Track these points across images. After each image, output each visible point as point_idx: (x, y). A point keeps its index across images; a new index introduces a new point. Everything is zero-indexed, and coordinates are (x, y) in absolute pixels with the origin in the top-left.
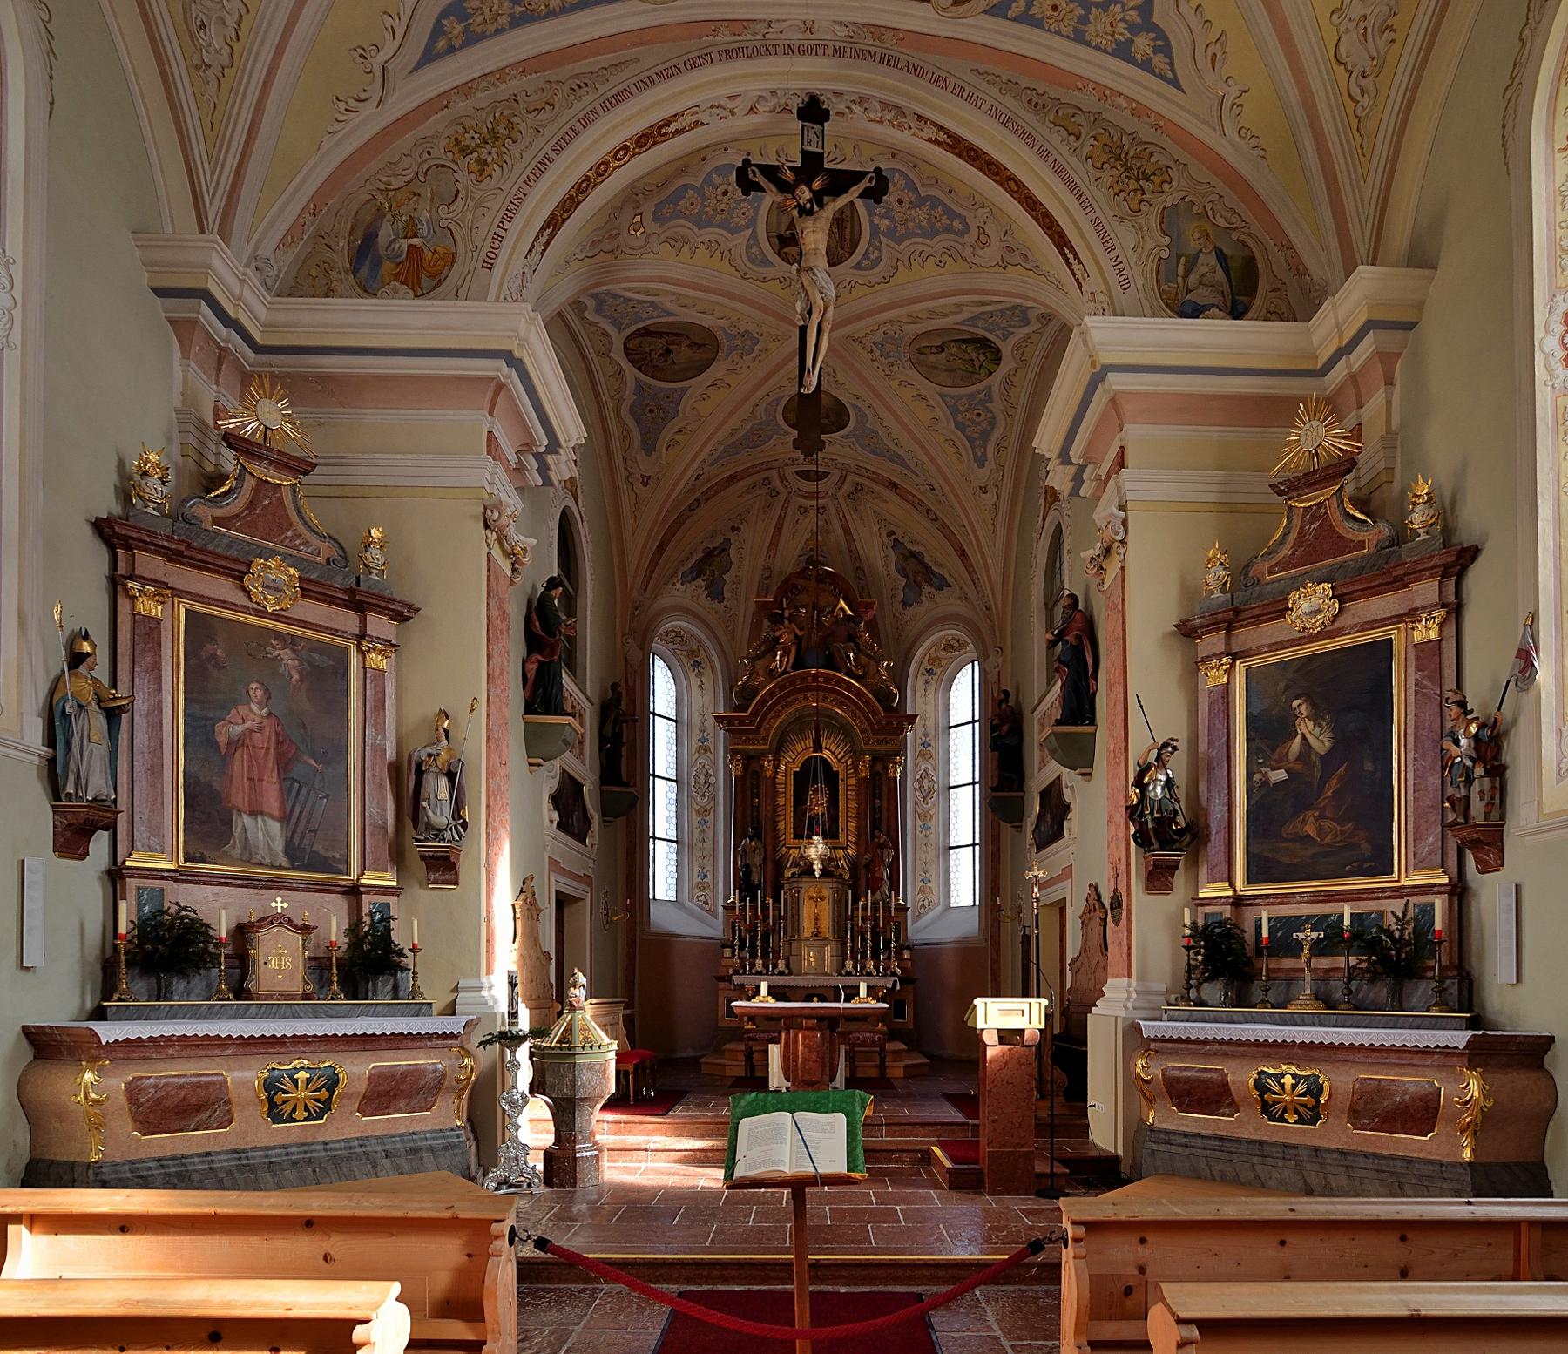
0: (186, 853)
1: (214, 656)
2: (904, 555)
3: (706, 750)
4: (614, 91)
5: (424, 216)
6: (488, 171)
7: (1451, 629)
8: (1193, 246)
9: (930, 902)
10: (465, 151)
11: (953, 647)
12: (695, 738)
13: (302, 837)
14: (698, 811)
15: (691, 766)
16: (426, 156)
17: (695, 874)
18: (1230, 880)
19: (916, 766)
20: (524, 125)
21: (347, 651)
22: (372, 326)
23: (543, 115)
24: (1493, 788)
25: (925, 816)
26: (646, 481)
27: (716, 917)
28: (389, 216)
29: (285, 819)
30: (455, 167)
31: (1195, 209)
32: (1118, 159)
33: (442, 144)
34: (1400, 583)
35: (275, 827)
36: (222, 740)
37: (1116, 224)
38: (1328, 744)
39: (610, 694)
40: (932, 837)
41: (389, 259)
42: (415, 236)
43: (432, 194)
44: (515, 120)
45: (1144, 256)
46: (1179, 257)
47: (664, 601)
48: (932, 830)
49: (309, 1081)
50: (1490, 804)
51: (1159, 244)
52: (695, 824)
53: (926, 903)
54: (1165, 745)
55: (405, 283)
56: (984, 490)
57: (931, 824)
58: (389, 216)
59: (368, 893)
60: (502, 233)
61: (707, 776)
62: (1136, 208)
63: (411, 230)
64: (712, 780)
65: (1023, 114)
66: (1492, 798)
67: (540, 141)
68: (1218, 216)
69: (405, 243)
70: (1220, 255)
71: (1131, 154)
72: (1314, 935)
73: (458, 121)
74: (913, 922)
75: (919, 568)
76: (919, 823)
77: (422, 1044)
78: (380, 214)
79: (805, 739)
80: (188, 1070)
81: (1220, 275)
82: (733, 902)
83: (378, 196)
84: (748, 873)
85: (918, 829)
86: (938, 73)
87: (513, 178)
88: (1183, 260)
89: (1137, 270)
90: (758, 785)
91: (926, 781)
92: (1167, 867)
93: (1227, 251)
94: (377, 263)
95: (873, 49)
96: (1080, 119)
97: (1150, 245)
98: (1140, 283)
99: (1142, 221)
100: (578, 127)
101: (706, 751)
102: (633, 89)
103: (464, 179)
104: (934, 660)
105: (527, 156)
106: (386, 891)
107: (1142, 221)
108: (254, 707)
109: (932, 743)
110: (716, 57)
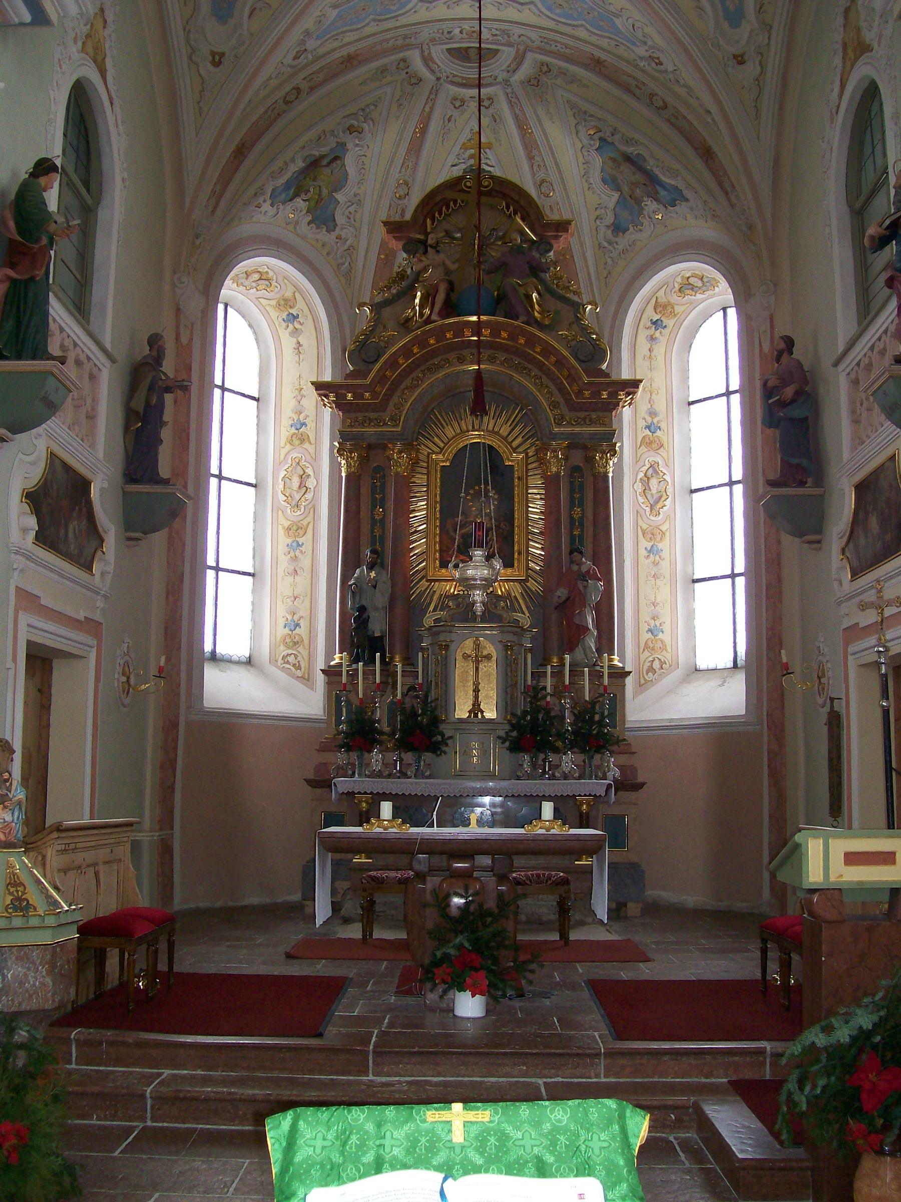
2: (614, 160)
3: (303, 439)
12: (286, 422)
14: (289, 529)
15: (278, 464)
17: (281, 622)
19: (637, 460)
25: (653, 534)
26: (217, 60)
27: (312, 687)
40: (665, 565)
47: (246, 228)
48: (665, 554)
52: (282, 548)
53: (656, 665)
56: (740, 60)
57: (664, 545)
61: (303, 477)
64: (311, 483)
74: (635, 695)
75: (639, 177)
76: (644, 544)
82: (340, 665)
85: (643, 553)
91: (654, 482)
104: (665, 307)
109: (663, 425)
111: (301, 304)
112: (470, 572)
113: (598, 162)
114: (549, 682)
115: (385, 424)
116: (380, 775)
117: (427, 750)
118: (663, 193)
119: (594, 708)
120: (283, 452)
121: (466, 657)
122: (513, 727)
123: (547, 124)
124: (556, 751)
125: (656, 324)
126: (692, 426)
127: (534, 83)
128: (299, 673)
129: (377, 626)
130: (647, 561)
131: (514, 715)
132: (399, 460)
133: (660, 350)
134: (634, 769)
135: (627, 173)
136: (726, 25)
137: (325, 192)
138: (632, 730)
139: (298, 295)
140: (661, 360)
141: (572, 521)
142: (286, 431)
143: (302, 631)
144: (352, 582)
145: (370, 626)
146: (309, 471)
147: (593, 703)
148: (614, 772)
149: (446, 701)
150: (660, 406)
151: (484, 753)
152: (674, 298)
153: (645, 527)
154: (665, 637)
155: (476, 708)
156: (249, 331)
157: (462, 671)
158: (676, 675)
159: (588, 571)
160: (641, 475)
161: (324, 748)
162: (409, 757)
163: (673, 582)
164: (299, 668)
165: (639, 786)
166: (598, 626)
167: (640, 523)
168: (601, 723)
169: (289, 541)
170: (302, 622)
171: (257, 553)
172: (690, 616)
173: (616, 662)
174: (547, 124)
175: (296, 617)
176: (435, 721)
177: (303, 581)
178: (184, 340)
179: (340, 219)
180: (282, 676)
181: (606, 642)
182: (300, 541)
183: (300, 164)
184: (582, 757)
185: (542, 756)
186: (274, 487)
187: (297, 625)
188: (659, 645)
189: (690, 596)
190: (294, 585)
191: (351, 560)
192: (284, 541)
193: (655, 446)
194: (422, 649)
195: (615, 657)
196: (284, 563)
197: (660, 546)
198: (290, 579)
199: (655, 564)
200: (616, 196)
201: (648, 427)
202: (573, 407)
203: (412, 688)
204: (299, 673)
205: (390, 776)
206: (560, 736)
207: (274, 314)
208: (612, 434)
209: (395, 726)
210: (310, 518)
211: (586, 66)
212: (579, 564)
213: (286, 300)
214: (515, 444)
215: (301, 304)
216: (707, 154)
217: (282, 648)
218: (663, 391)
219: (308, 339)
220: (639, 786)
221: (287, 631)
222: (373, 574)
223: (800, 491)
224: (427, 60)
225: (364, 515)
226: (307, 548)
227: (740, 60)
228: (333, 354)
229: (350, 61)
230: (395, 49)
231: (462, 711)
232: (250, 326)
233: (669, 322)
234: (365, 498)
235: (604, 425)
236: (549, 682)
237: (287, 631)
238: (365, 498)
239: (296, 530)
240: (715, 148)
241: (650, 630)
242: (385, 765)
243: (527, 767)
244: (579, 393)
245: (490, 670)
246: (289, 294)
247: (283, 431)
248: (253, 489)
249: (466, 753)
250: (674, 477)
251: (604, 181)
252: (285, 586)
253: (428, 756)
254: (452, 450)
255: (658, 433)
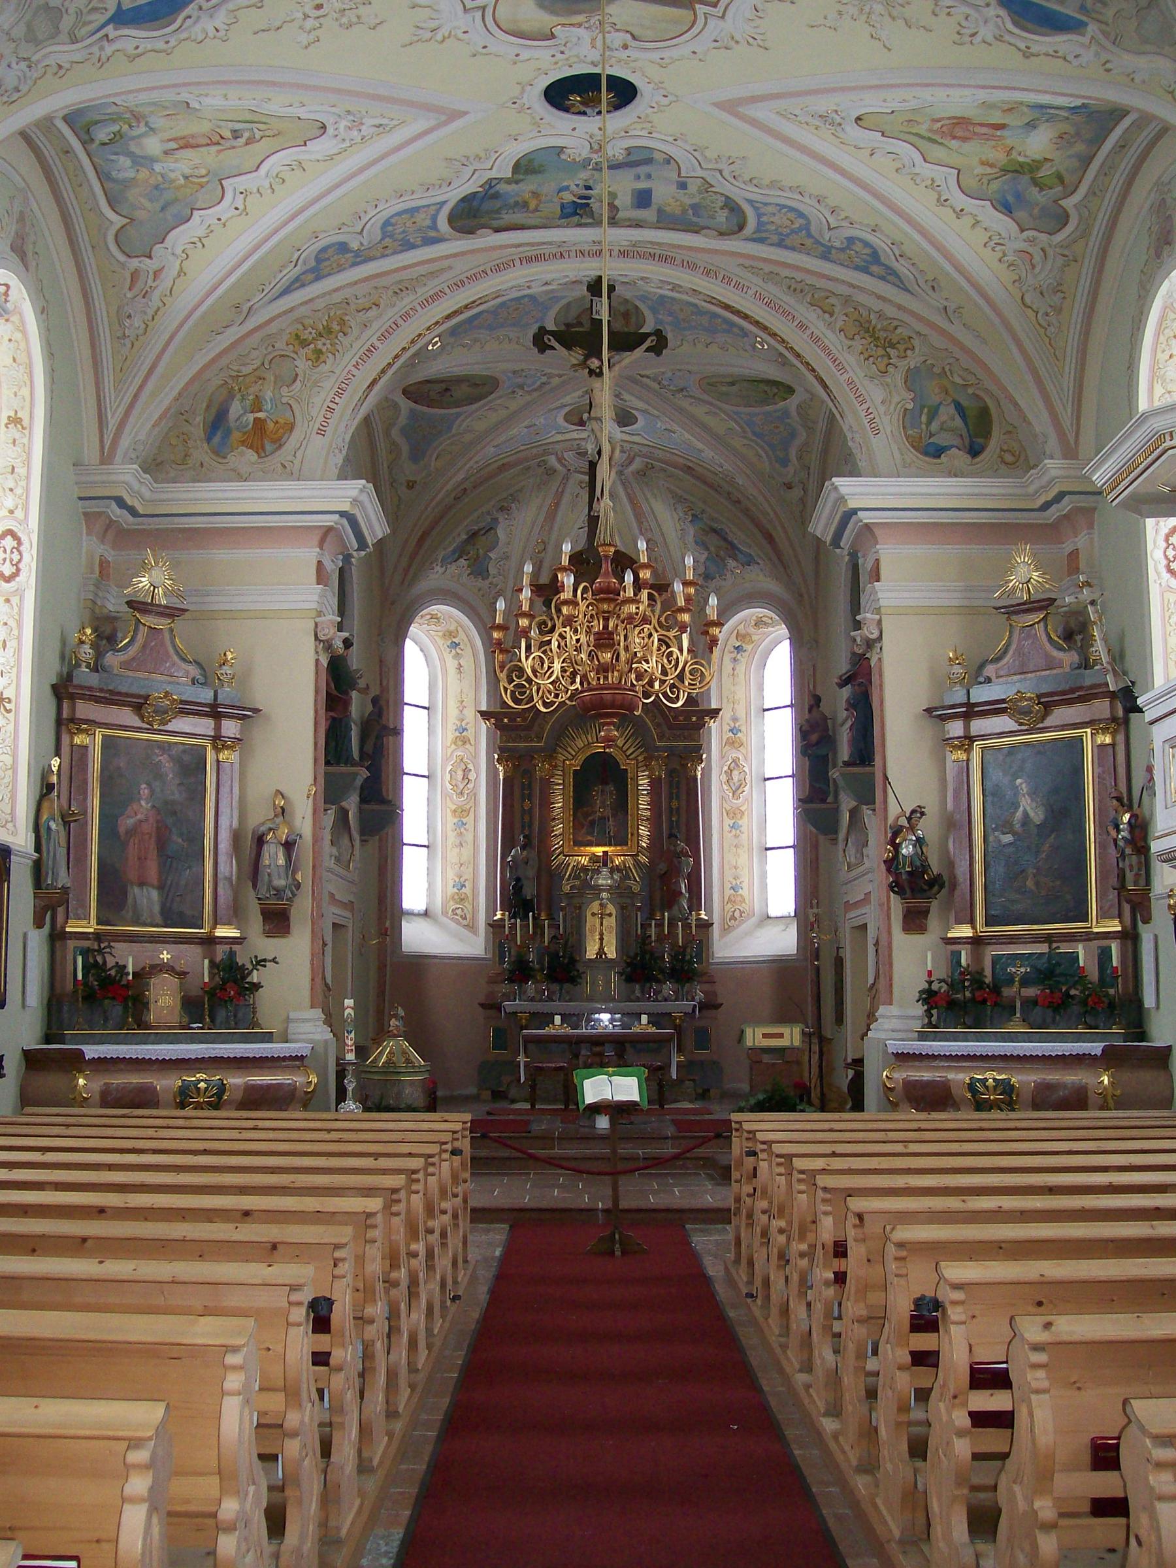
0: (98, 918)
1: (119, 768)
2: (704, 530)
3: (465, 741)
4: (431, 293)
5: (268, 395)
6: (323, 358)
7: (1120, 738)
8: (935, 399)
9: (741, 913)
10: (304, 344)
11: (765, 624)
12: (451, 727)
13: (172, 901)
14: (455, 811)
15: (445, 760)
16: (270, 348)
17: (451, 884)
18: (972, 922)
19: (722, 756)
20: (353, 321)
21: (205, 747)
22: (233, 499)
23: (370, 314)
24: (1140, 863)
25: (735, 813)
26: (411, 485)
27: (475, 933)
28: (238, 396)
29: (161, 888)
30: (295, 356)
31: (935, 370)
32: (867, 331)
33: (285, 337)
34: (1084, 699)
35: (155, 894)
36: (122, 830)
37: (866, 382)
38: (1042, 817)
39: (370, 708)
40: (744, 837)
41: (238, 429)
42: (260, 411)
43: (276, 377)
44: (347, 318)
45: (892, 408)
46: (922, 407)
47: (423, 585)
48: (744, 829)
49: (206, 1089)
50: (1137, 875)
51: (903, 398)
52: (450, 826)
53: (737, 914)
54: (913, 812)
55: (251, 447)
56: (789, 486)
57: (744, 822)
58: (238, 396)
59: (221, 943)
60: (333, 406)
61: (466, 771)
62: (883, 369)
63: (257, 406)
64: (472, 776)
65: (784, 298)
66: (1139, 869)
67: (369, 332)
68: (955, 375)
69: (251, 417)
70: (959, 407)
71: (879, 327)
72: (1023, 970)
73: (299, 321)
74: (722, 936)
75: (722, 543)
76: (728, 822)
77: (278, 1064)
78: (231, 396)
79: (586, 733)
80: (135, 1079)
81: (958, 422)
82: (502, 920)
83: (230, 381)
84: (518, 889)
85: (726, 828)
86: (710, 267)
87: (344, 363)
88: (926, 410)
89: (886, 420)
90: (530, 785)
91: (735, 773)
92: (920, 912)
93: (965, 403)
94: (228, 433)
95: (652, 251)
96: (832, 300)
97: (896, 399)
98: (888, 430)
99: (889, 380)
100: (400, 322)
101: (465, 743)
102: (447, 290)
103: (302, 365)
104: (744, 636)
105: (357, 345)
106: (234, 941)
107: (889, 380)
108: (143, 803)
109: (743, 728)
110: (517, 263)
111: (462, 635)
112: (600, 882)
113: (691, 531)
114: (653, 932)
115: (532, 741)
116: (532, 1000)
117: (567, 981)
118: (740, 556)
119: (685, 950)
120: (449, 751)
121: (593, 914)
122: (629, 964)
123: (652, 501)
124: (658, 981)
125: (738, 649)
126: (765, 728)
127: (642, 474)
128: (465, 923)
129: (529, 891)
130: (730, 835)
131: (628, 957)
132: (541, 768)
133: (741, 668)
134: (715, 994)
135: (714, 541)
136: (777, 466)
137: (481, 552)
138: (717, 964)
139: (460, 629)
140: (742, 676)
141: (671, 810)
142: (451, 735)
143: (467, 890)
144: (509, 859)
145: (524, 891)
146: (470, 766)
147: (684, 947)
148: (700, 995)
149: (580, 946)
150: (741, 713)
151: (608, 983)
152: (752, 630)
153: (728, 808)
154: (744, 892)
155: (601, 951)
156: (421, 654)
157: (591, 922)
158: (753, 920)
159: (681, 851)
160: (726, 768)
161: (492, 981)
162: (555, 987)
163: (750, 850)
164: (465, 918)
165: (718, 1006)
166: (689, 890)
167: (725, 805)
168: (691, 963)
169: (456, 820)
170: (467, 884)
171: (430, 829)
172: (764, 875)
173: (703, 916)
174: (652, 501)
175: (462, 880)
176: (573, 961)
177: (467, 852)
178: (385, 683)
179: (492, 571)
180: (453, 925)
181: (695, 901)
182: (465, 820)
183: (464, 537)
184: (676, 986)
185: (648, 985)
186: (443, 777)
187: (463, 886)
188: (739, 898)
189: (764, 861)
190: (460, 855)
191: (508, 844)
192: (451, 820)
193: (736, 745)
194: (562, 909)
195: (703, 912)
196: (452, 837)
197: (740, 822)
198: (457, 850)
199: (736, 836)
200: (706, 554)
201: (731, 731)
202: (671, 727)
203: (554, 937)
204: (465, 923)
205: (541, 1000)
206: (662, 971)
207: (440, 642)
208: (700, 747)
209: (543, 965)
210: (471, 804)
211: (681, 470)
212: (676, 845)
213: (450, 633)
214: (628, 753)
215: (462, 635)
216: (770, 538)
217: (452, 903)
218: (743, 702)
219: (467, 662)
220: (718, 1006)
221: (455, 890)
222: (525, 853)
223: (823, 806)
224: (560, 460)
225: (517, 806)
226: (470, 826)
227: (789, 486)
228: (488, 683)
229: (504, 467)
230: (535, 457)
231: (591, 952)
232: (422, 650)
233: (749, 647)
234: (517, 795)
235: (694, 741)
236: (653, 932)
237: (455, 890)
238: (517, 795)
239: (461, 813)
240: (774, 534)
241: (732, 888)
242: (537, 991)
243: (638, 993)
244: (675, 718)
245: (611, 922)
246: (452, 628)
247: (449, 733)
248: (426, 780)
249: (593, 983)
250: (751, 768)
251: (696, 543)
252: (453, 855)
253: (567, 986)
254: (582, 757)
255: (739, 735)
